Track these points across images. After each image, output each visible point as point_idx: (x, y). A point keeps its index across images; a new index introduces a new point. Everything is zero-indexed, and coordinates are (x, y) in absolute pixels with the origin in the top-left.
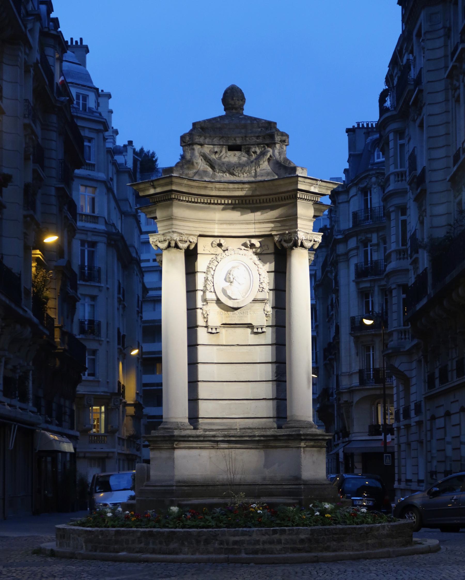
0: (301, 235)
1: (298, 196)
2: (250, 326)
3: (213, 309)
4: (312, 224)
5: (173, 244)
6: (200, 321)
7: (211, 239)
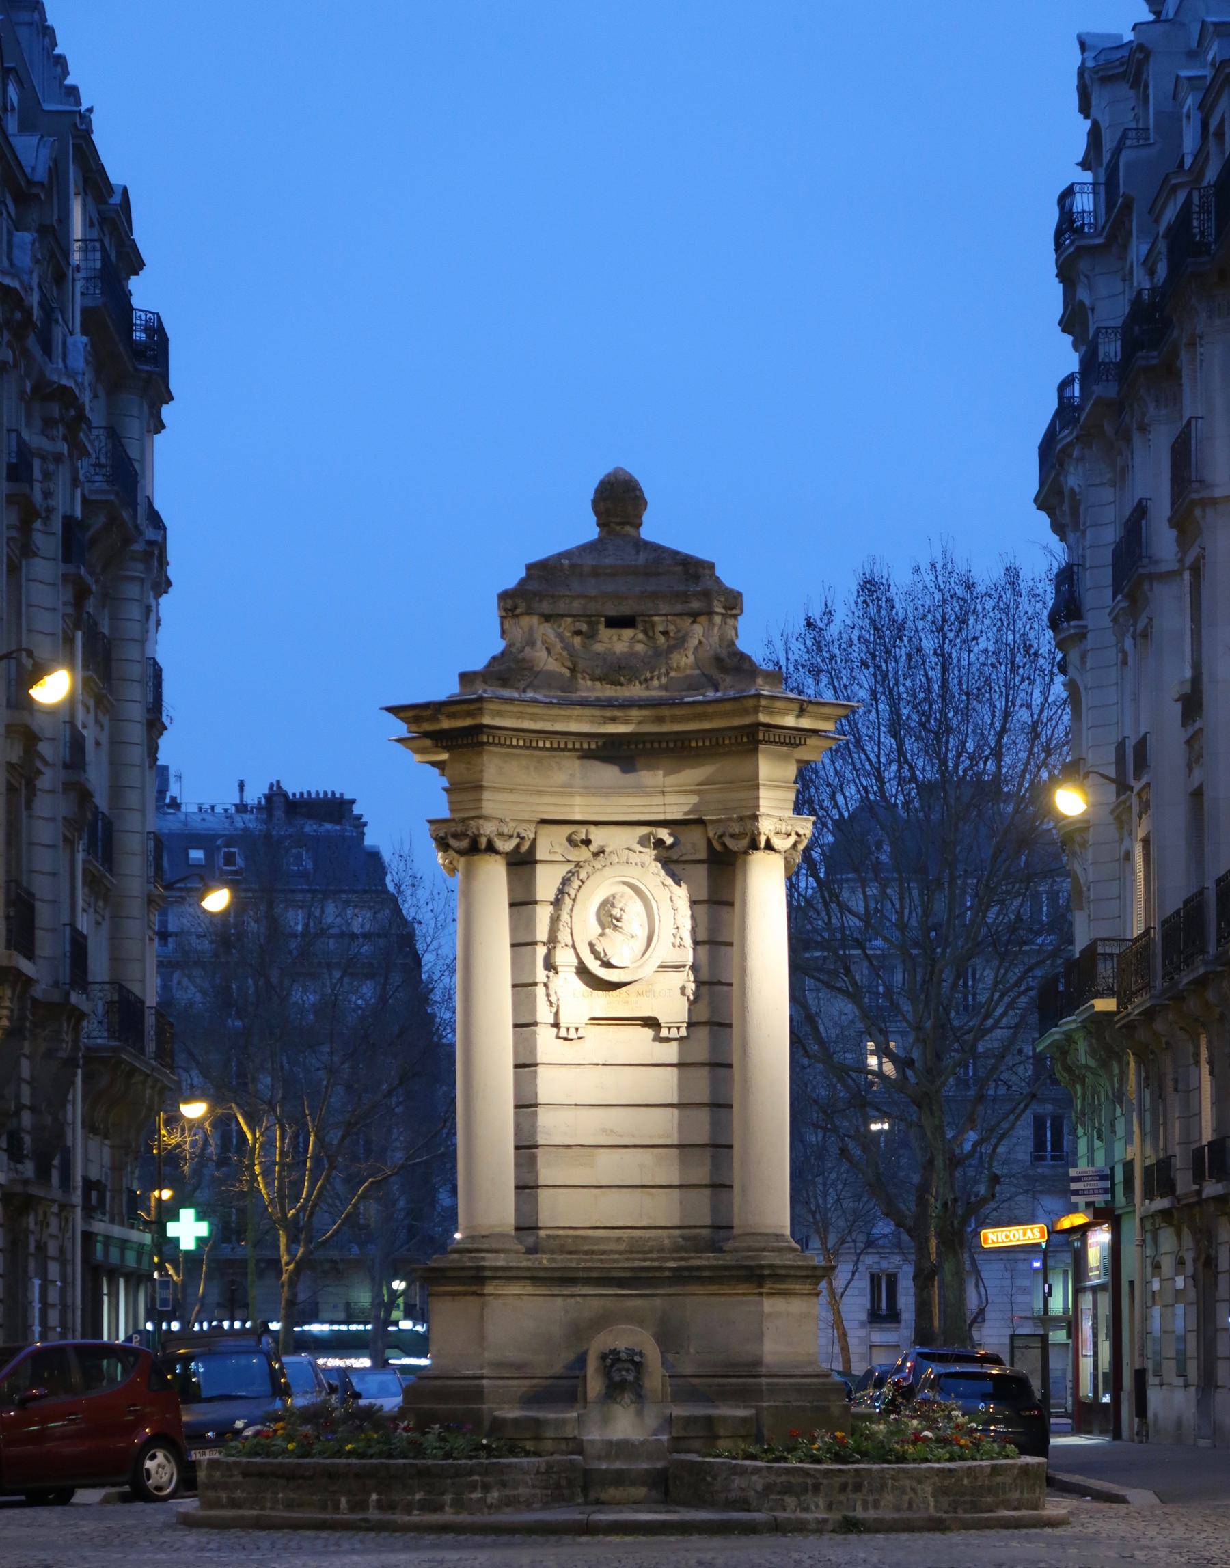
0: (766, 827)
1: (761, 737)
3: (567, 984)
4: (792, 796)
5: (483, 841)
6: (544, 1014)
7: (567, 830)
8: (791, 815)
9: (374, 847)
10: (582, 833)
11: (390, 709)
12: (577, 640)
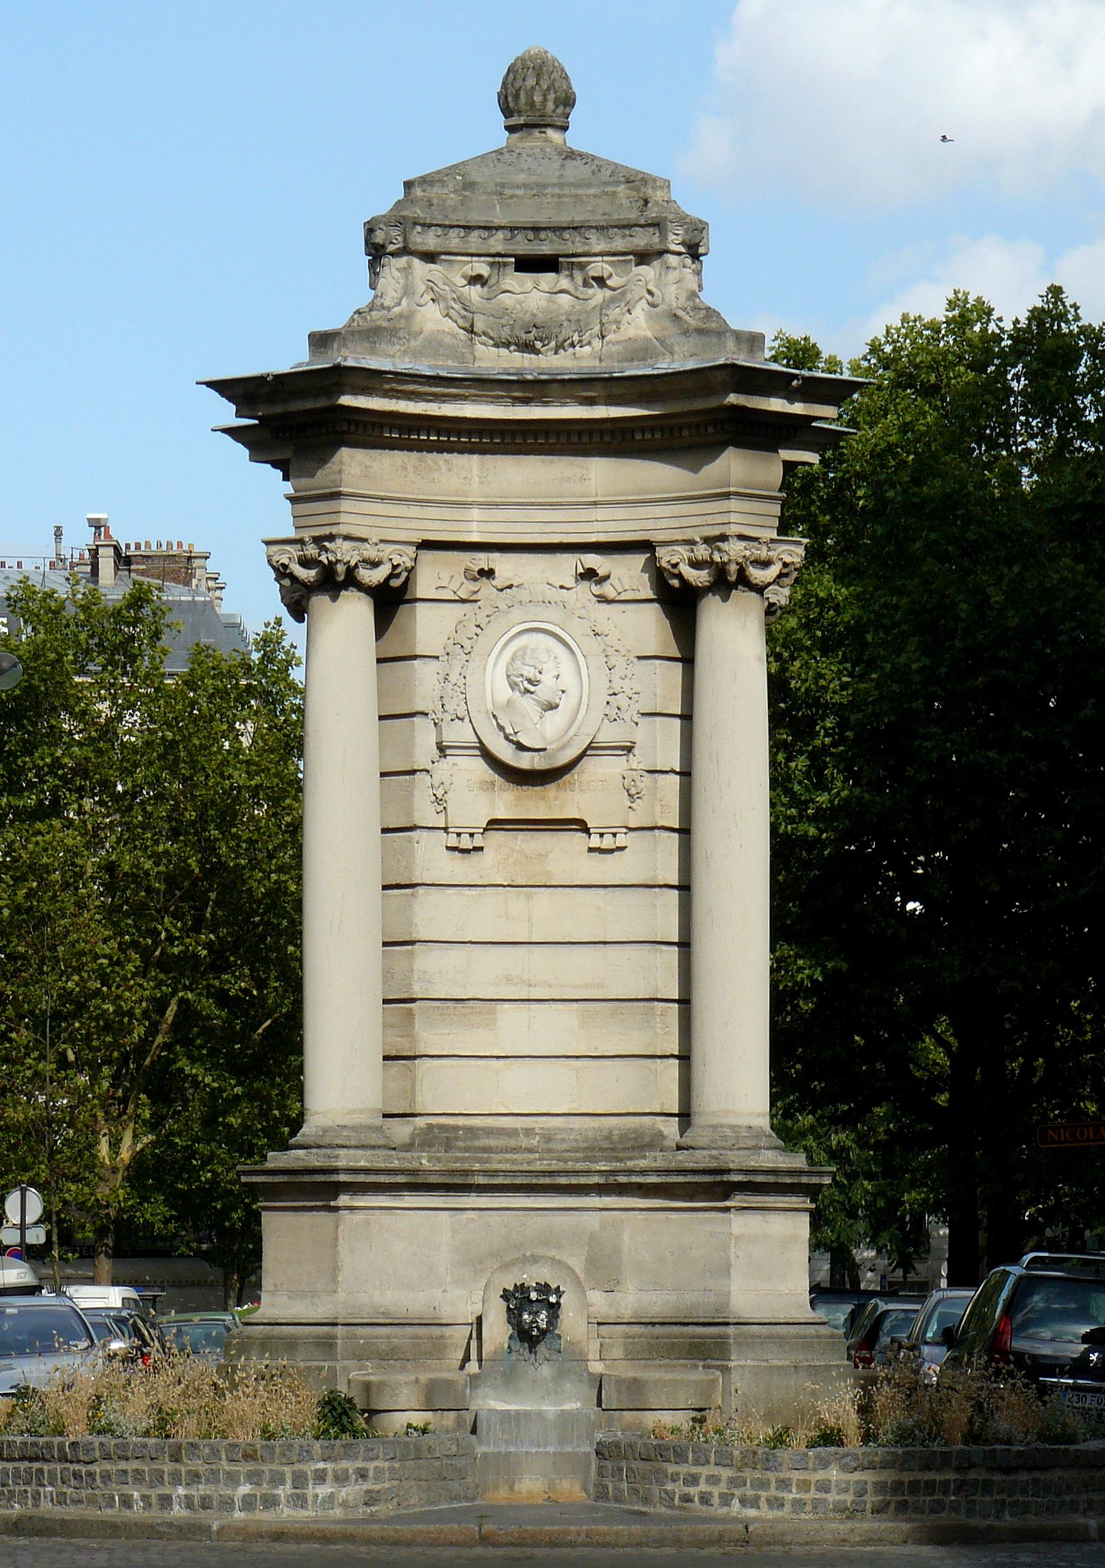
2: (582, 826)
8: (774, 535)
9: (233, 616)
10: (482, 560)
11: (210, 384)
12: (475, 293)
